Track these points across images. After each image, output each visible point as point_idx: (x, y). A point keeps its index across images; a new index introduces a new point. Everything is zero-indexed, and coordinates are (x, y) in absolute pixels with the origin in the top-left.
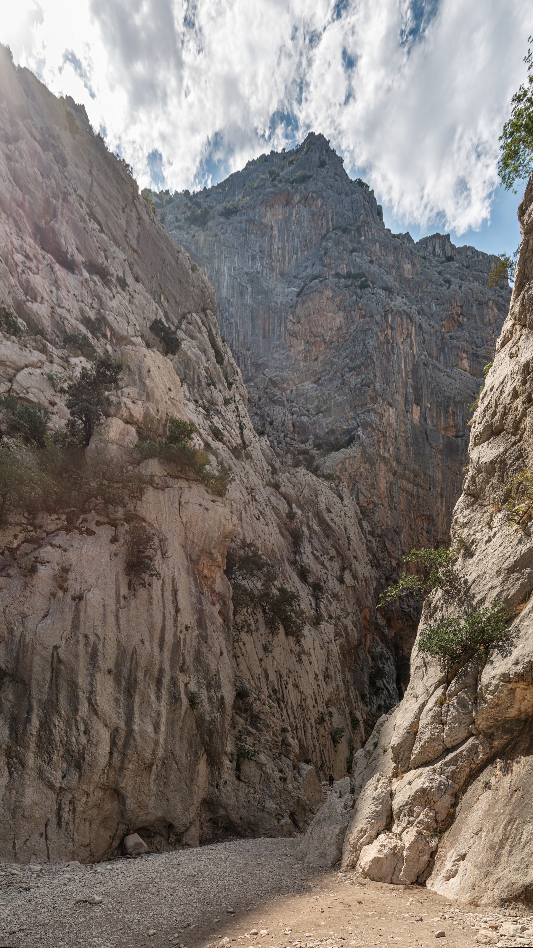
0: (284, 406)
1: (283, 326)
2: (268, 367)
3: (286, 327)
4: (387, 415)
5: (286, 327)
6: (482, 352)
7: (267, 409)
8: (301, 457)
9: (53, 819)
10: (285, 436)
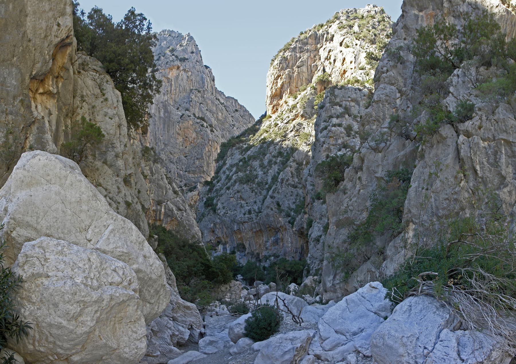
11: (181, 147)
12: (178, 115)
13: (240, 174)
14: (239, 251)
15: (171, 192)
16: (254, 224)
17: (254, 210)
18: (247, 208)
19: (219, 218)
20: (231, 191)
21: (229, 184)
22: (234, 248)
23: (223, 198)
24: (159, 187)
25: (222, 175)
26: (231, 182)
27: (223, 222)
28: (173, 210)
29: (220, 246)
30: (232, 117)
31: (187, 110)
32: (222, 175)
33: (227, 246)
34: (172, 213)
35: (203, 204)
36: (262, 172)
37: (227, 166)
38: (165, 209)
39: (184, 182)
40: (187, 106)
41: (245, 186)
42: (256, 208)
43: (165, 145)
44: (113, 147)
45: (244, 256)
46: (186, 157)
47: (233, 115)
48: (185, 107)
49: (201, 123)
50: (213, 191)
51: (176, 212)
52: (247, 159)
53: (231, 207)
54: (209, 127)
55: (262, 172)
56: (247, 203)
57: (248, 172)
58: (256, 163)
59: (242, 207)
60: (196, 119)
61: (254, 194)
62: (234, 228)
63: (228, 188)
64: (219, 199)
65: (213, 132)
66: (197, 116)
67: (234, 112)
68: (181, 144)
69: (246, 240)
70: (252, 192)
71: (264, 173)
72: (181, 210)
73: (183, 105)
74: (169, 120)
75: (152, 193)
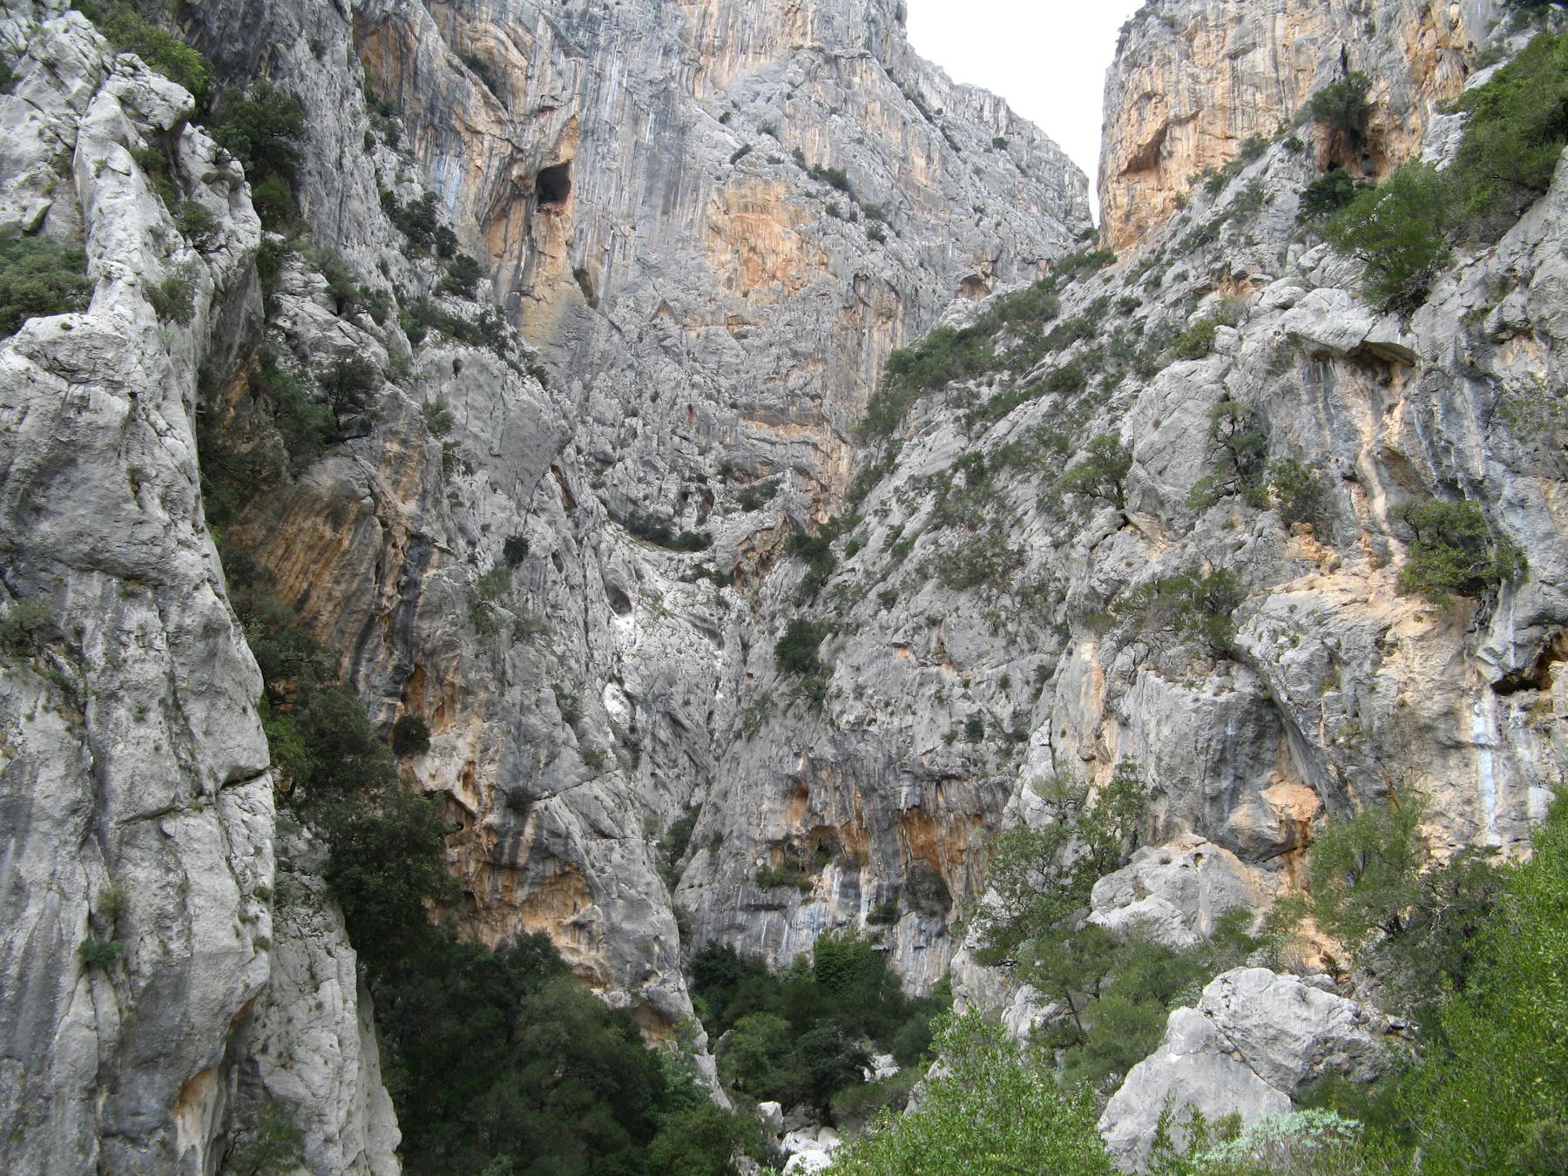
0: (680, 363)
1: (701, 205)
2: (663, 275)
3: (704, 210)
4: (835, 456)
5: (704, 210)
6: (715, 990)
7: (649, 361)
8: (693, 486)
9: (691, 558)
10: (673, 432)
11: (722, 291)
12: (724, 144)
13: (952, 538)
14: (915, 906)
15: (569, 758)
16: (990, 789)
17: (996, 724)
18: (965, 709)
19: (833, 741)
20: (899, 613)
21: (894, 580)
22: (896, 889)
23: (863, 646)
24: (524, 736)
25: (872, 520)
26: (902, 569)
27: (848, 763)
28: (568, 836)
29: (828, 870)
30: (978, 171)
31: (769, 132)
32: (872, 520)
33: (863, 876)
34: (566, 845)
35: (771, 650)
36: (1048, 539)
37: (899, 480)
38: (539, 827)
39: (718, 452)
40: (772, 113)
41: (963, 600)
42: (1003, 710)
43: (646, 267)
44: (321, 1121)
45: (940, 935)
46: (740, 336)
47: (982, 163)
48: (755, 117)
49: (829, 200)
50: (824, 592)
51: (579, 842)
52: (986, 462)
53: (895, 692)
54: (861, 215)
55: (1048, 539)
56: (966, 684)
57: (983, 532)
58: (1023, 492)
59: (940, 700)
60: (804, 176)
61: (1000, 642)
62: (896, 794)
63: (888, 600)
64: (842, 648)
65: (882, 240)
66: (811, 162)
67: (988, 150)
68: (723, 275)
69: (952, 860)
70: (994, 633)
71: (1056, 545)
72: (604, 835)
73: (749, 108)
74: (679, 160)
75: (492, 760)
